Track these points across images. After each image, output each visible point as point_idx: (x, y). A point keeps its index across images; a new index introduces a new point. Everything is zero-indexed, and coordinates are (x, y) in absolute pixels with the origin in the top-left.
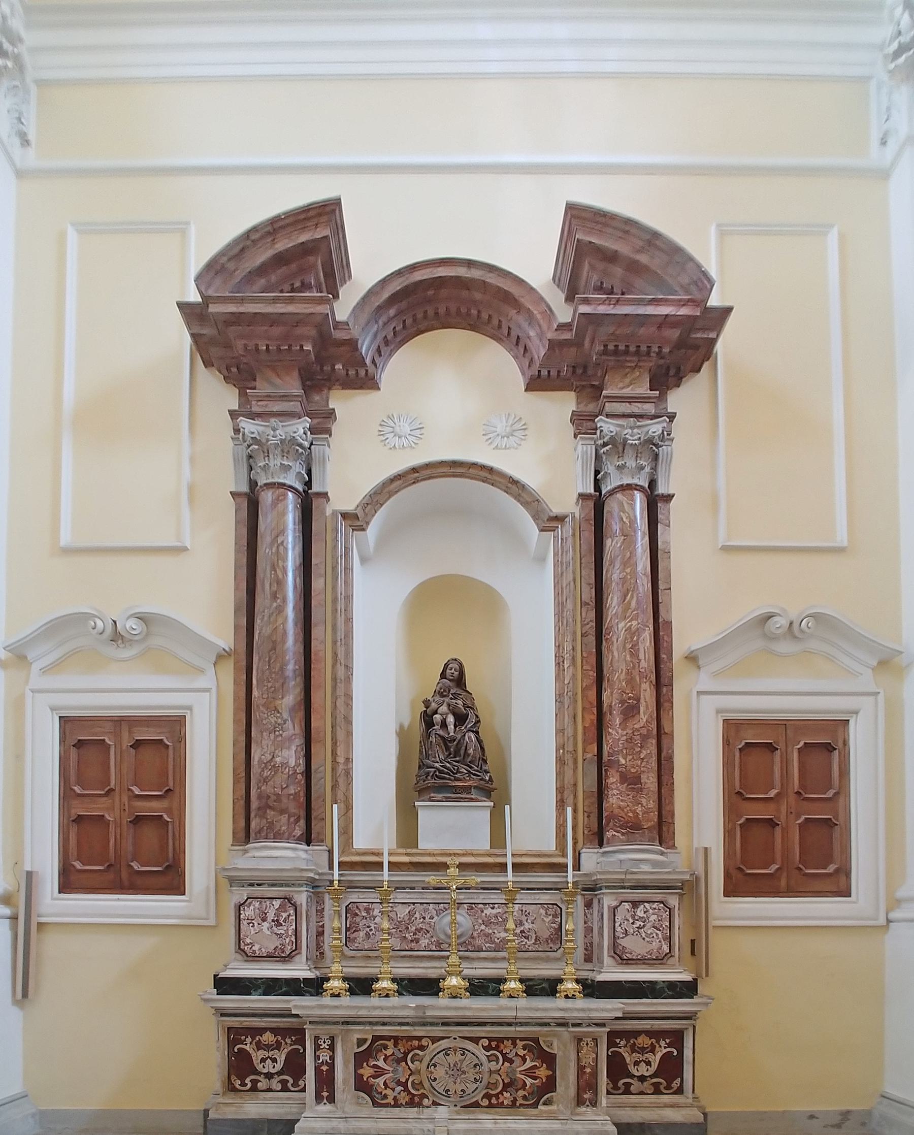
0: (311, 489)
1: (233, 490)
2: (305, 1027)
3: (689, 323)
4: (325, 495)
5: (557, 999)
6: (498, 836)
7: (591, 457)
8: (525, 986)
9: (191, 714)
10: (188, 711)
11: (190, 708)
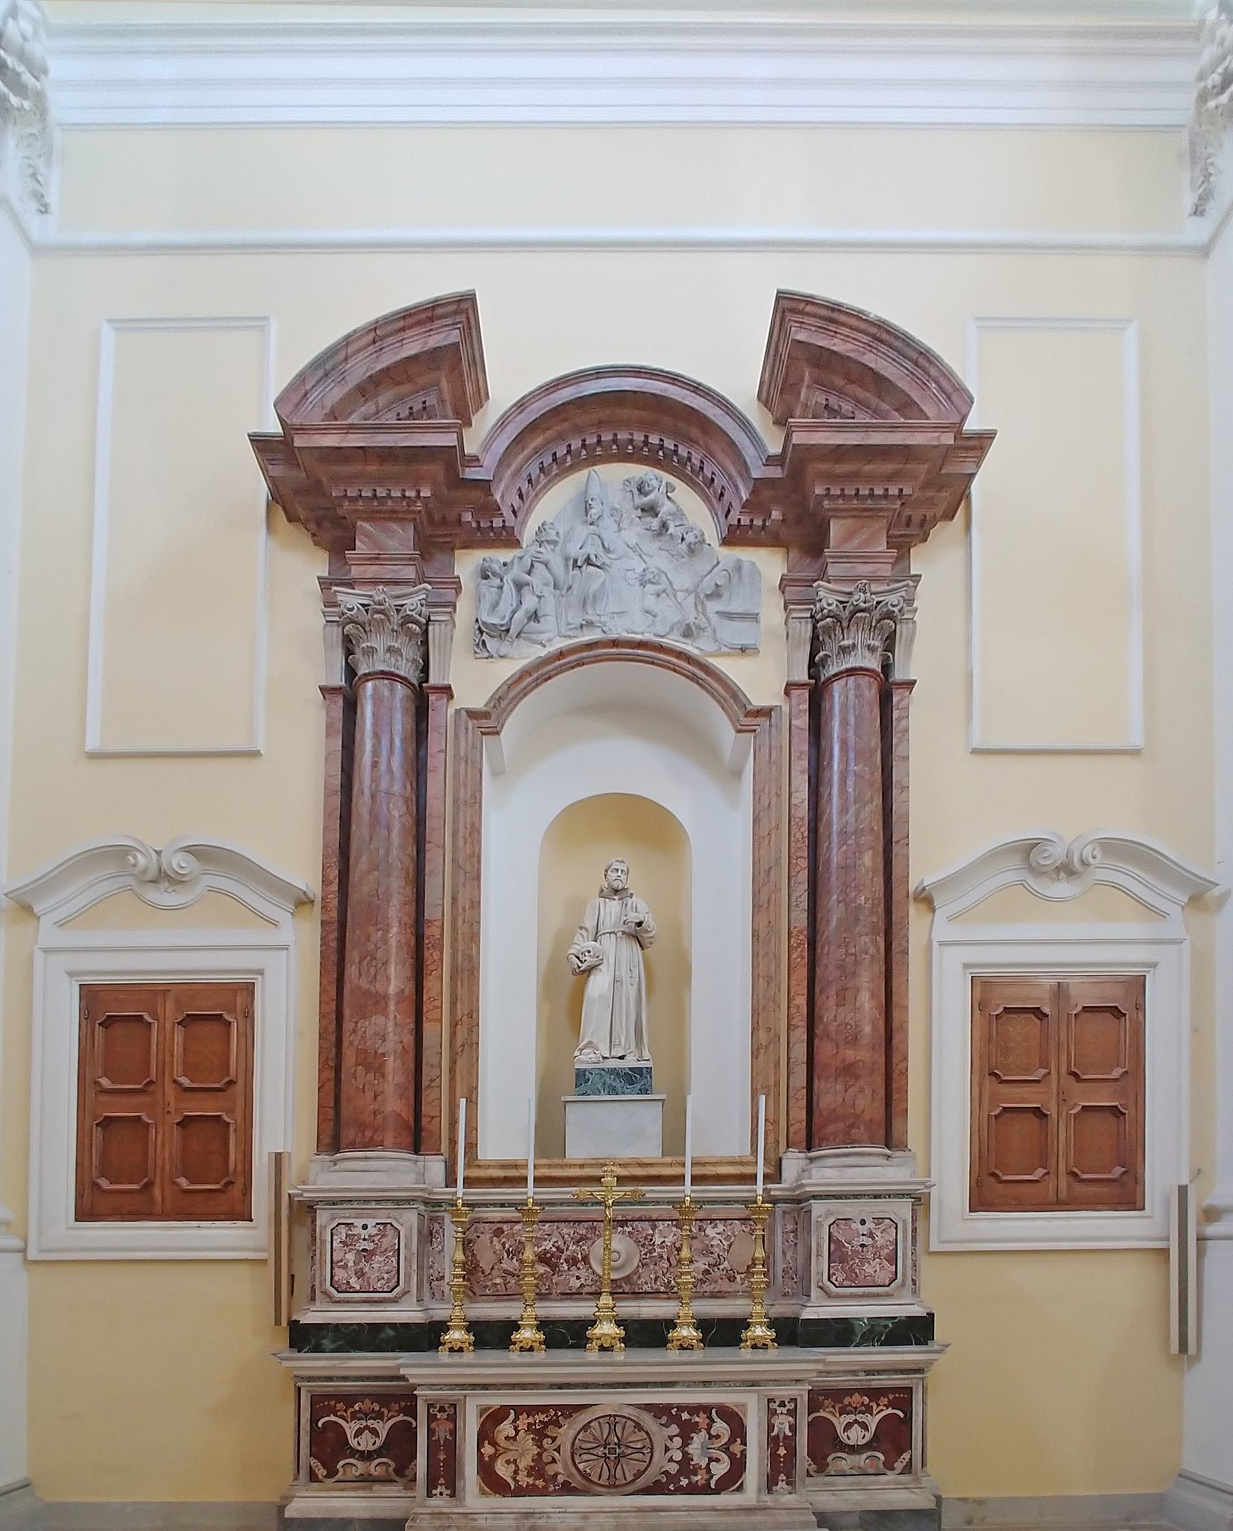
0: (427, 682)
1: (323, 683)
2: (415, 1393)
3: (947, 453)
4: (447, 691)
5: (511, 1353)
6: (674, 1139)
7: (434, 642)
8: (544, 1334)
9: (263, 979)
10: (259, 977)
11: (261, 972)
